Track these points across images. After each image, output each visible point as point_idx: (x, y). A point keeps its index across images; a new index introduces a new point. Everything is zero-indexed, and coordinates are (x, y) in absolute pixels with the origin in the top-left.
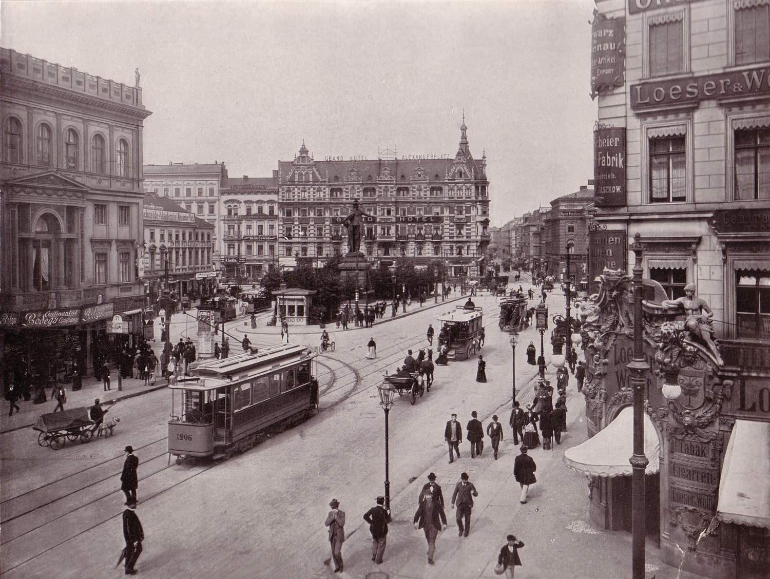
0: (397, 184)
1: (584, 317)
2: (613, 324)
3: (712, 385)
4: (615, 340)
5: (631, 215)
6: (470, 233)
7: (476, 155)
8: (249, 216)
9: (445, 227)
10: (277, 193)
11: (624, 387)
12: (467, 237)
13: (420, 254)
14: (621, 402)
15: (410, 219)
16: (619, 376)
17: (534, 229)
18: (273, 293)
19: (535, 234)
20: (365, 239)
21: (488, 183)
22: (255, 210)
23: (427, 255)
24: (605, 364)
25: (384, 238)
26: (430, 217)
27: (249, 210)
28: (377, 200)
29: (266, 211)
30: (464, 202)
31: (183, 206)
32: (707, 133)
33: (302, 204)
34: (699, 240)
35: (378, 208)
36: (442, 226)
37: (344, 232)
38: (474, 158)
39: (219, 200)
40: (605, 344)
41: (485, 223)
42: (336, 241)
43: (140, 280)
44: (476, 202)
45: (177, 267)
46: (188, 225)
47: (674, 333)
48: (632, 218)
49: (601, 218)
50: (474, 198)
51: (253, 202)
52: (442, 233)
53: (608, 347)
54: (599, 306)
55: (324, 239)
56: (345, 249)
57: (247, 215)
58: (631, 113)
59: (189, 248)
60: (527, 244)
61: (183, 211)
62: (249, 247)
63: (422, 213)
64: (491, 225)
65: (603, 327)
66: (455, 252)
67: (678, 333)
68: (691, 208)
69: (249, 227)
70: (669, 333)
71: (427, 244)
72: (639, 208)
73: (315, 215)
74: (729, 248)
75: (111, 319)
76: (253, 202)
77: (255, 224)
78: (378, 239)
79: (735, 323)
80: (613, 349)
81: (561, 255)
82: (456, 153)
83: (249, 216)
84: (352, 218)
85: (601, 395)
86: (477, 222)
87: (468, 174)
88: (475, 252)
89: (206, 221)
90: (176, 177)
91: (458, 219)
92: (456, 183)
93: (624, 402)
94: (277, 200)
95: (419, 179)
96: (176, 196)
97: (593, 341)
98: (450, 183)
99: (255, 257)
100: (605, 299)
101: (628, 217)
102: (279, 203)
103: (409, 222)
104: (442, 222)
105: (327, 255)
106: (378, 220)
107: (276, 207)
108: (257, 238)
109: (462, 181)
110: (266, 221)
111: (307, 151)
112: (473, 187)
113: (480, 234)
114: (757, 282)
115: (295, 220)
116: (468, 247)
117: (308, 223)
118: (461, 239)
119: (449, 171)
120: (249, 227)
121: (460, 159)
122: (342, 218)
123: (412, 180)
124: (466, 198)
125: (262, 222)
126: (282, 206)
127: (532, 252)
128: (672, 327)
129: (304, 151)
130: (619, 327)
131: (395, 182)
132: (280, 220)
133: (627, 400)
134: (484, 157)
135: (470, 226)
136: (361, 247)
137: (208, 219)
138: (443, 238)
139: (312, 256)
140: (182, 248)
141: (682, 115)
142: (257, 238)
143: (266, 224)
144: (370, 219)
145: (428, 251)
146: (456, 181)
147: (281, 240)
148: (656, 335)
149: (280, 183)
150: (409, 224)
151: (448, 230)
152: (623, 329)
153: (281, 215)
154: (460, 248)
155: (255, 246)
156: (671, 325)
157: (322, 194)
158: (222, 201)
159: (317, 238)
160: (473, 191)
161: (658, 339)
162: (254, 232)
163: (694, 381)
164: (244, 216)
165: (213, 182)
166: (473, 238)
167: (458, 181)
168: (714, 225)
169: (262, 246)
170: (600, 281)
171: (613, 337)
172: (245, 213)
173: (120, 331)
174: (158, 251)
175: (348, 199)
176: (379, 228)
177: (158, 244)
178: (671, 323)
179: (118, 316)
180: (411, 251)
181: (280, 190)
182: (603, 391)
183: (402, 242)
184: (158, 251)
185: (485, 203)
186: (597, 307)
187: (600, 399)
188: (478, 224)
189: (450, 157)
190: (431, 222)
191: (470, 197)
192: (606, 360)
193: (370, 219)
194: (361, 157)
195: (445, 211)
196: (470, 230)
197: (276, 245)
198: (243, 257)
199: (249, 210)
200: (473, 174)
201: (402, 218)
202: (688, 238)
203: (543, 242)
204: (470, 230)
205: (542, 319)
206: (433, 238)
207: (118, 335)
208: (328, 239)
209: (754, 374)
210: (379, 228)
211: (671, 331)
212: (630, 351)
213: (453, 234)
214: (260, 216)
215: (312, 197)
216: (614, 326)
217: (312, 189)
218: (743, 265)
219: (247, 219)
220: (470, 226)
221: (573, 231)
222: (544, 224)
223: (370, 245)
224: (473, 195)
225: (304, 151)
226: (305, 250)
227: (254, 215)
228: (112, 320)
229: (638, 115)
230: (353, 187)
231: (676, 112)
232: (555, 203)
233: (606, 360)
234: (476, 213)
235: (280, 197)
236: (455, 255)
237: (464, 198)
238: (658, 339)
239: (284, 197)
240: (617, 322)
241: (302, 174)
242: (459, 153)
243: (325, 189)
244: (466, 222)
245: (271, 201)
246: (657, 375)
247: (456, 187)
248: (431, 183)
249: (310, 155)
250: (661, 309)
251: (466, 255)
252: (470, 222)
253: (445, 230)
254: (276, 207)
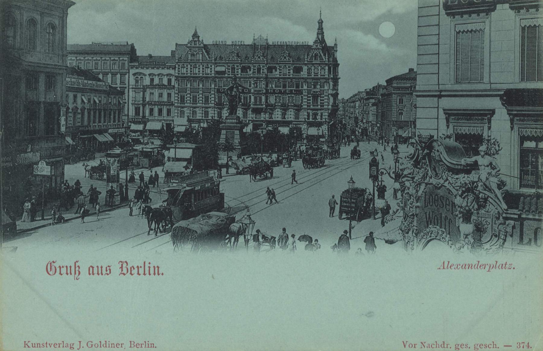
0: (267, 64)
1: (402, 170)
2: (424, 175)
3: (498, 224)
4: (425, 189)
5: (441, 91)
6: (323, 103)
7: (329, 42)
8: (152, 86)
9: (304, 97)
10: (174, 68)
11: (431, 224)
12: (321, 106)
13: (284, 118)
14: (428, 237)
15: (277, 91)
16: (428, 216)
17: (373, 101)
18: (167, 146)
19: (373, 105)
20: (242, 106)
21: (339, 64)
22: (156, 81)
23: (290, 119)
24: (417, 207)
25: (256, 105)
26: (292, 90)
27: (152, 80)
28: (252, 75)
29: (165, 81)
30: (319, 79)
31: (101, 76)
32: (437, 27)
33: (193, 77)
34: (492, 112)
35: (252, 82)
36: (302, 97)
37: (225, 99)
38: (328, 45)
39: (129, 73)
40: (417, 191)
41: (335, 96)
42: (220, 105)
43: (62, 133)
44: (329, 79)
45: (104, 124)
46: (104, 92)
47: (470, 183)
48: (443, 93)
49: (419, 94)
50: (327, 76)
51: (155, 75)
52: (302, 103)
53: (420, 193)
54: (414, 162)
55: (210, 105)
56: (225, 113)
57: (151, 85)
58: (443, 12)
59: (118, 110)
60: (367, 112)
61: (99, 80)
62: (151, 110)
63: (274, 86)
64: (340, 97)
65: (416, 178)
66: (311, 117)
67: (473, 184)
68: (488, 87)
69: (152, 94)
70: (465, 183)
71: (276, 110)
72: (447, 86)
73: (191, 86)
74: (513, 117)
75: (37, 163)
76: (155, 75)
77: (156, 92)
78: (252, 106)
79: (519, 177)
80: (424, 195)
81: (393, 121)
82: (314, 41)
83: (152, 86)
84: (231, 89)
85: (413, 231)
86: (329, 94)
87: (323, 57)
88: (327, 117)
89: (119, 89)
90: (96, 54)
91: (314, 92)
92: (313, 64)
93: (431, 237)
94: (174, 74)
95: (259, 60)
96: (95, 69)
97: (409, 188)
98: (309, 64)
99: (156, 118)
100: (418, 156)
101: (439, 93)
102: (175, 76)
103: (277, 93)
104: (302, 94)
105: (212, 117)
106: (252, 91)
107: (173, 79)
108: (157, 103)
109: (317, 62)
110: (157, 90)
111: (199, 37)
112: (327, 68)
113: (331, 104)
114: (537, 145)
115: (200, 89)
116: (322, 114)
117: (186, 92)
118: (316, 107)
119: (308, 55)
120: (152, 94)
121: (317, 46)
122: (224, 89)
123: (279, 61)
124: (321, 76)
125: (162, 90)
126: (177, 78)
127: (371, 119)
128: (469, 179)
129: (195, 35)
130: (428, 178)
131: (266, 62)
132: (176, 89)
133: (432, 235)
134: (336, 45)
135: (323, 97)
136: (238, 112)
137: (120, 88)
138: (302, 106)
139: (201, 118)
140: (99, 109)
141: (482, 15)
142: (157, 103)
143: (165, 93)
144: (246, 90)
145: (290, 116)
146: (313, 62)
147: (176, 104)
148: (456, 185)
149: (177, 61)
150: (277, 95)
151: (306, 100)
152: (431, 180)
153: (176, 86)
154: (315, 115)
155: (156, 110)
156: (468, 177)
157: (209, 70)
158: (131, 74)
159: (193, 104)
160: (327, 71)
161: (458, 188)
162: (165, 98)
163: (485, 221)
164: (148, 85)
165: (125, 59)
166: (326, 107)
167: (315, 62)
168: (504, 100)
169: (153, 109)
170: (415, 142)
171: (424, 185)
172: (148, 83)
173: (44, 173)
174: (79, 111)
175: (281, 75)
176: (252, 98)
177: (80, 106)
178: (468, 176)
179: (42, 161)
180: (277, 115)
181: (177, 66)
182: (415, 228)
183: (271, 108)
184: (79, 111)
185: (336, 80)
186: (412, 162)
187: (412, 234)
188: (330, 96)
189: (309, 44)
190: (293, 94)
191: (324, 76)
192: (418, 204)
193: (246, 90)
194: (240, 42)
195: (304, 85)
196: (323, 100)
197: (173, 109)
198: (147, 117)
199: (152, 80)
200: (327, 57)
201: (271, 90)
202: (485, 110)
203: (380, 111)
204: (323, 100)
205: (374, 171)
206: (282, 106)
207: (44, 176)
208: (213, 105)
209: (531, 216)
210: (252, 98)
211: (467, 182)
212: (436, 197)
213: (310, 103)
214: (161, 86)
215: (201, 72)
216: (424, 177)
217: (189, 66)
218: (528, 132)
219: (150, 88)
220: (323, 97)
221: (402, 103)
222: (380, 97)
223: (246, 110)
224: (327, 73)
225: (195, 35)
226: (194, 113)
227: (156, 85)
228: (38, 164)
229: (448, 14)
230: (285, 66)
231: (478, 13)
232: (389, 81)
233: (418, 204)
234: (328, 88)
235: (177, 71)
236: (311, 120)
237: (319, 76)
238: (458, 188)
239: (281, 73)
240: (427, 174)
241: (194, 54)
242: (316, 41)
243: (211, 66)
244: (321, 94)
245: (170, 74)
246: (457, 216)
247: (313, 67)
248: (294, 64)
249: (200, 39)
250: (461, 165)
251: (319, 120)
252: (323, 94)
253: (304, 100)
254: (173, 79)
